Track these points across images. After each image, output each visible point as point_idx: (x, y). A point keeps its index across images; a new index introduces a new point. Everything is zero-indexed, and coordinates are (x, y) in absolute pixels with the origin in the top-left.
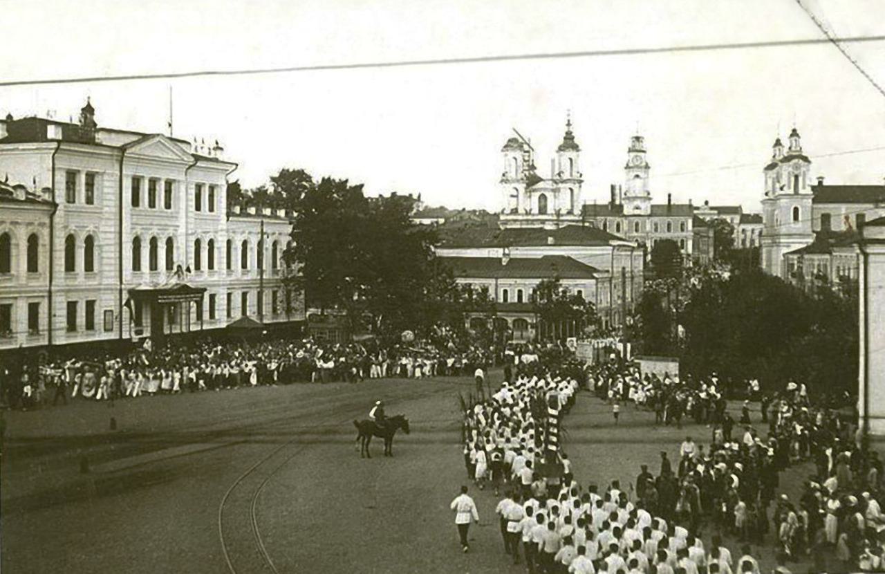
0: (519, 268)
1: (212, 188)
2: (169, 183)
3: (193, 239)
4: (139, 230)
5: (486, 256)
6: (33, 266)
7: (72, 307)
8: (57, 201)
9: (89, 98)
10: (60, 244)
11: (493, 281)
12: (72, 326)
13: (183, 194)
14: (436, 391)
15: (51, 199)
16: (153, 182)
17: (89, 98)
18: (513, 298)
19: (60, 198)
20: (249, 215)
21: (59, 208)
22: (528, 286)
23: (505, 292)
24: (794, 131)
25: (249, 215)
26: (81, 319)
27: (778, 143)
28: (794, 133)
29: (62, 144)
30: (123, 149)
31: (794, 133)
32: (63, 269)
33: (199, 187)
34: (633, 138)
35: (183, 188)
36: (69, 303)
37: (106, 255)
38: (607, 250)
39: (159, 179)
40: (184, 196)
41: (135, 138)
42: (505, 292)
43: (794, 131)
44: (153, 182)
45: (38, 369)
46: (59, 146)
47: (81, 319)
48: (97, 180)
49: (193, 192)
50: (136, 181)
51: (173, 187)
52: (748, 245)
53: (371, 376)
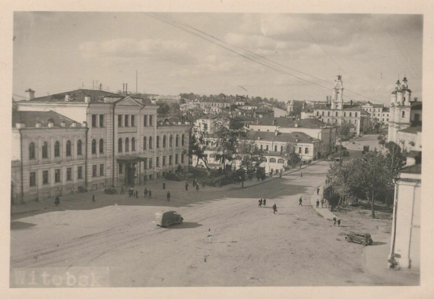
0: (279, 136)
3: (143, 137)
4: (95, 137)
5: (99, 148)
6: (79, 153)
7: (94, 167)
8: (88, 127)
11: (271, 142)
14: (92, 260)
15: (70, 127)
19: (90, 126)
20: (167, 125)
21: (89, 130)
22: (280, 145)
26: (98, 172)
27: (398, 82)
28: (405, 80)
29: (90, 104)
30: (114, 104)
31: (405, 80)
32: (91, 153)
33: (145, 117)
34: (404, 141)
37: (108, 146)
39: (148, 115)
40: (139, 121)
41: (119, 99)
44: (127, 117)
46: (89, 105)
47: (98, 172)
48: (136, 117)
49: (143, 118)
50: (120, 117)
52: (334, 197)
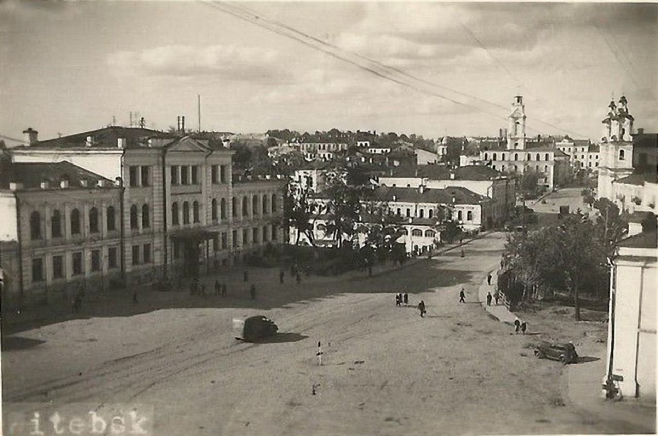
1: (222, 167)
2: (195, 168)
4: (134, 201)
7: (135, 249)
9: (114, 117)
10: (127, 210)
11: (414, 204)
12: (135, 261)
13: (204, 173)
16: (184, 168)
17: (114, 117)
18: (426, 215)
19: (126, 184)
22: (428, 208)
23: (422, 211)
24: (623, 98)
25: (248, 181)
26: (141, 257)
35: (204, 169)
36: (133, 247)
38: (224, 156)
40: (205, 175)
42: (422, 211)
43: (623, 98)
44: (184, 168)
45: (446, 229)
47: (141, 257)
50: (174, 169)
51: (225, 168)
53: (570, 213)
